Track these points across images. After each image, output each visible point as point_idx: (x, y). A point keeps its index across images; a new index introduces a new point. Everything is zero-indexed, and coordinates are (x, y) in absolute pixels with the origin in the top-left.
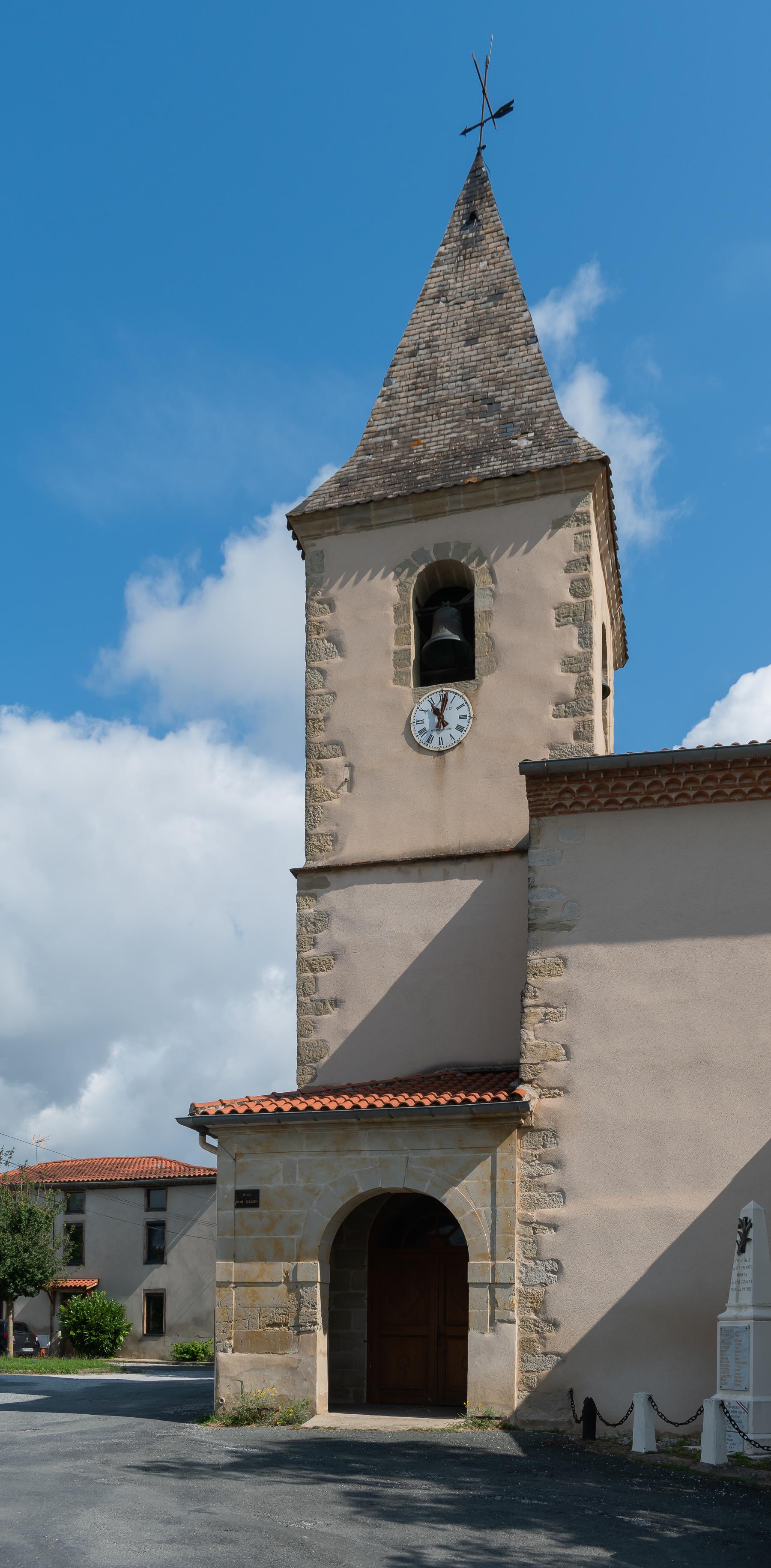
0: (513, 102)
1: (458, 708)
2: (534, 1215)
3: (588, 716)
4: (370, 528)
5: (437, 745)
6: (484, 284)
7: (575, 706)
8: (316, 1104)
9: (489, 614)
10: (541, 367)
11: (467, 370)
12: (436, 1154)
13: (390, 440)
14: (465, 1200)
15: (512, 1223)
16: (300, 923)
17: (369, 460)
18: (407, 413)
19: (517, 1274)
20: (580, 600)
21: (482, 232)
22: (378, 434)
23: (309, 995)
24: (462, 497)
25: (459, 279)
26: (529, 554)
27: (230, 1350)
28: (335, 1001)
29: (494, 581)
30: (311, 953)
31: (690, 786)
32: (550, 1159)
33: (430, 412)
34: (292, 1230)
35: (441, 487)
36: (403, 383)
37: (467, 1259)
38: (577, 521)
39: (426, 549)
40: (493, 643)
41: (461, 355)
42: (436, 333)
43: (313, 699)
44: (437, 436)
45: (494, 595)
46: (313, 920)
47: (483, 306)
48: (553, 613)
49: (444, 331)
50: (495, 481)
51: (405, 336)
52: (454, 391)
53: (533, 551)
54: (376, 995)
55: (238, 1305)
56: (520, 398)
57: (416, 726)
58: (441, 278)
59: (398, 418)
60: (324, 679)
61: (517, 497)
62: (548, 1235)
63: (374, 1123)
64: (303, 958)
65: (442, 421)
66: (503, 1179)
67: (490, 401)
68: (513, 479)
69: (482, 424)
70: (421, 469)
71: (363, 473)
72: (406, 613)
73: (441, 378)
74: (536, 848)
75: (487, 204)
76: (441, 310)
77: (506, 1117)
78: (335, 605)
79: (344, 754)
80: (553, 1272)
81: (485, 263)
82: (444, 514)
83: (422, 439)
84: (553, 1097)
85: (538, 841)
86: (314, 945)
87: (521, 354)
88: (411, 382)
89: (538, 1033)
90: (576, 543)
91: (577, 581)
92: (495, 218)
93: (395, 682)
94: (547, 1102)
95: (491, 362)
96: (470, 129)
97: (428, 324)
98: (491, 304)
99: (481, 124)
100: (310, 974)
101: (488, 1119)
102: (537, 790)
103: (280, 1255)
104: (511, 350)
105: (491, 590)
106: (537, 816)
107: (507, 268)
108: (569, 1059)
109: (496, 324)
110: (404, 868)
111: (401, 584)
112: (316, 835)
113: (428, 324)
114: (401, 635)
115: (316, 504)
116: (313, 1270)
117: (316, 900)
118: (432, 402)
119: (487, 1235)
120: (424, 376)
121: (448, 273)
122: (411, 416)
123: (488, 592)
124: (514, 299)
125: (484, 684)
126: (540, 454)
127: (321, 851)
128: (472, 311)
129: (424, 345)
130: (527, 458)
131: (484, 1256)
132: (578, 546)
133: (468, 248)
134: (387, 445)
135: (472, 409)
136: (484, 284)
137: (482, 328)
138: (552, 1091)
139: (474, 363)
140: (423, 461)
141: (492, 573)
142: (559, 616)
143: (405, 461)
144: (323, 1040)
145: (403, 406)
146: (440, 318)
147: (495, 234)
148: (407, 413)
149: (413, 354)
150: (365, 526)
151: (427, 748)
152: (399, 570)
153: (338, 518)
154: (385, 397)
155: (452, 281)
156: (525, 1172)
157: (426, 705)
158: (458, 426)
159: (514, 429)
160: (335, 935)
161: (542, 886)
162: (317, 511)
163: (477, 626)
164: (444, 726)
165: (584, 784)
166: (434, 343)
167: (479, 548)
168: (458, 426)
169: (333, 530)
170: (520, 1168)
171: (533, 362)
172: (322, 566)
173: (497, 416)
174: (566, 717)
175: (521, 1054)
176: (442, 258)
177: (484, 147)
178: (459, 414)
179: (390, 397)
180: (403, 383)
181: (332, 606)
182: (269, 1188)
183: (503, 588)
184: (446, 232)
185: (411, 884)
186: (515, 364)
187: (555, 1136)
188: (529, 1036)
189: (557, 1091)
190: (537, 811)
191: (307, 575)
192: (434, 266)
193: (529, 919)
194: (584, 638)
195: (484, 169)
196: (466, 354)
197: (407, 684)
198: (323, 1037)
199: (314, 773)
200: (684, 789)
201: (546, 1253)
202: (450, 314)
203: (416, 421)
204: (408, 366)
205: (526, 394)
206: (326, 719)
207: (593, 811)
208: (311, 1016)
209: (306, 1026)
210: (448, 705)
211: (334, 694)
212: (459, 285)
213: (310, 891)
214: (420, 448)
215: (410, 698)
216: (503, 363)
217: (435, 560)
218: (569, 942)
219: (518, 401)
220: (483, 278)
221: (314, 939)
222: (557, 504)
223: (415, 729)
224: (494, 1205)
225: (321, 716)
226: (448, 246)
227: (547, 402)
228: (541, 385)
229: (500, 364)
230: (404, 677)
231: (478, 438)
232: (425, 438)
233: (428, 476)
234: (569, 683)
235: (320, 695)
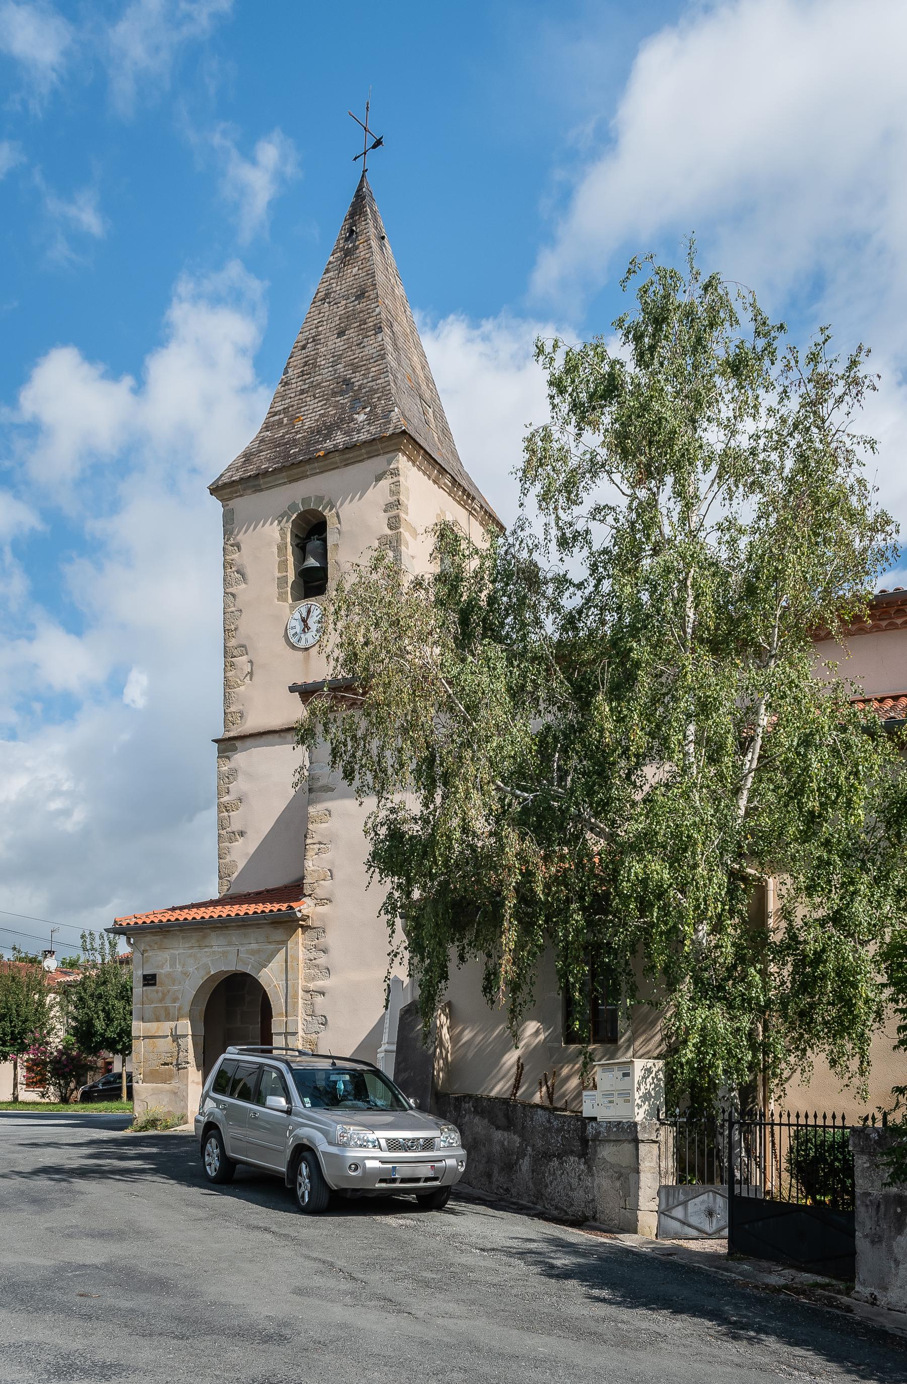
2: (311, 986)
4: (262, 490)
12: (254, 946)
14: (270, 977)
15: (297, 992)
19: (300, 1026)
21: (357, 243)
22: (275, 414)
27: (140, 1082)
30: (226, 799)
32: (321, 947)
34: (175, 1000)
36: (295, 372)
37: (271, 1017)
42: (320, 329)
54: (266, 826)
55: (145, 1051)
62: (319, 999)
65: (317, 400)
73: (319, 366)
80: (322, 1024)
82: (307, 477)
94: (320, 909)
97: (316, 322)
98: (357, 302)
99: (365, 153)
100: (226, 814)
101: (281, 923)
103: (168, 1018)
110: (282, 734)
113: (316, 322)
114: (283, 565)
115: (225, 479)
116: (185, 1026)
119: (283, 1001)
122: (297, 398)
123: (336, 530)
131: (281, 1014)
132: (392, 493)
134: (280, 422)
141: (338, 516)
150: (258, 489)
152: (280, 519)
155: (334, 285)
156: (306, 957)
160: (239, 786)
168: (325, 404)
175: (303, 878)
176: (330, 266)
179: (286, 384)
180: (295, 372)
182: (162, 972)
183: (345, 527)
197: (286, 601)
199: (229, 668)
201: (318, 1012)
206: (236, 629)
208: (227, 844)
212: (338, 288)
218: (332, 799)
219: (365, 381)
222: (376, 464)
223: (291, 632)
224: (287, 980)
225: (233, 627)
226: (336, 256)
228: (381, 367)
229: (357, 352)
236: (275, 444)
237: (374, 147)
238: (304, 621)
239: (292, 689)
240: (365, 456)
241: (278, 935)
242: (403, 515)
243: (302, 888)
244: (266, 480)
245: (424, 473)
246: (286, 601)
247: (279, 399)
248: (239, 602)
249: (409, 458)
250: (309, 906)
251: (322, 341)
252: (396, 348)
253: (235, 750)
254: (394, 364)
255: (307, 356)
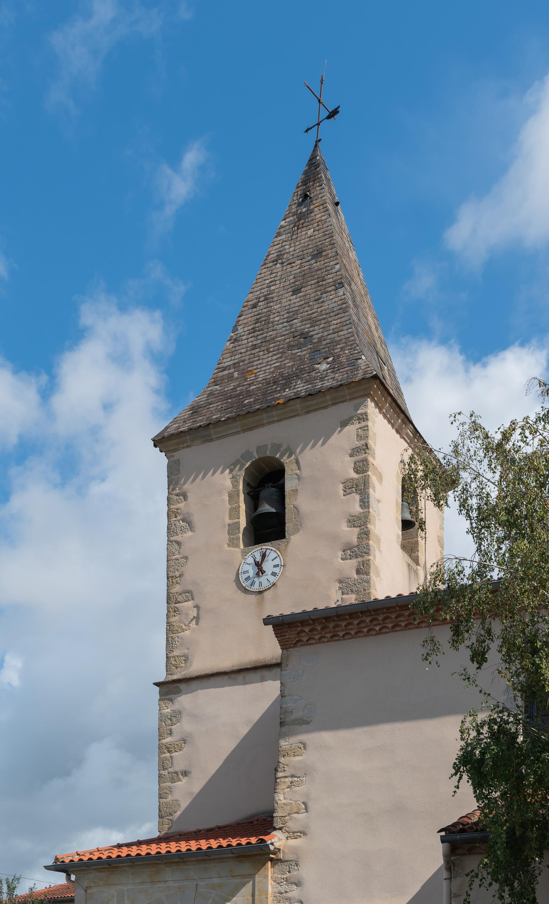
0: (339, 107)
1: (272, 560)
3: (366, 557)
4: (212, 440)
5: (258, 587)
6: (310, 246)
7: (359, 550)
8: (173, 847)
9: (295, 491)
10: (344, 306)
11: (292, 314)
12: (216, 881)
13: (233, 373)
16: (161, 720)
17: (216, 390)
18: (247, 351)
20: (361, 475)
21: (312, 207)
22: (224, 369)
23: (167, 769)
24: (274, 413)
25: (292, 245)
26: (324, 447)
28: (185, 772)
29: (299, 469)
30: (168, 740)
31: (388, 621)
32: (293, 880)
33: (262, 349)
35: (259, 409)
36: (246, 329)
38: (358, 420)
39: (251, 451)
40: (298, 512)
41: (289, 302)
42: (273, 288)
43: (172, 563)
44: (265, 366)
45: (299, 478)
46: (169, 717)
47: (308, 263)
48: (341, 486)
49: (278, 286)
50: (297, 400)
51: (250, 293)
52: (281, 331)
53: (326, 445)
56: (326, 331)
57: (243, 575)
58: (280, 245)
59: (240, 355)
60: (180, 548)
61: (314, 408)
63: (174, 862)
64: (163, 744)
65: (270, 354)
66: (260, 895)
67: (306, 336)
68: (310, 397)
69: (298, 354)
70: (249, 394)
71: (210, 401)
72: (237, 497)
73: (272, 322)
74: (286, 670)
75: (318, 184)
76: (278, 270)
77: (260, 854)
78: (187, 496)
79: (193, 599)
81: (312, 230)
82: (263, 425)
83: (255, 369)
84: (296, 838)
85: (287, 665)
86: (170, 734)
87: (331, 297)
88: (252, 327)
89: (286, 796)
90: (358, 435)
91: (358, 462)
92: (322, 195)
93: (229, 545)
94: (292, 842)
95: (309, 306)
96: (311, 128)
97: (267, 282)
98: (313, 261)
99: (318, 124)
100: (168, 755)
101: (248, 856)
102: (281, 633)
104: (324, 295)
105: (297, 474)
106: (286, 649)
107: (327, 233)
108: (307, 812)
109: (316, 277)
111: (233, 477)
112: (174, 657)
113: (267, 282)
115: (171, 431)
117: (172, 702)
118: (265, 341)
120: (261, 322)
121: (285, 241)
122: (249, 353)
123: (295, 476)
124: (330, 255)
125: (292, 541)
126: (332, 375)
127: (177, 668)
128: (299, 268)
129: (263, 298)
130: (322, 379)
133: (301, 219)
134: (230, 377)
135: (292, 343)
136: (310, 246)
137: (305, 280)
138: (296, 834)
139: (297, 308)
140: (251, 388)
141: (297, 462)
142: (345, 488)
143: (240, 388)
144: (176, 800)
145: (244, 346)
146: (276, 276)
147: (321, 207)
148: (247, 351)
149: (255, 306)
150: (208, 439)
151: (251, 590)
152: (232, 467)
153: (188, 437)
154: (232, 341)
155: (287, 247)
156: (276, 890)
157: (250, 560)
158: (281, 357)
159: (320, 355)
161: (289, 695)
162: (172, 435)
163: (287, 500)
164: (262, 573)
165: (313, 626)
166: (270, 296)
167: (288, 446)
168: (281, 357)
169: (185, 445)
170: (271, 887)
171: (339, 302)
172: (179, 470)
173: (309, 346)
174: (350, 559)
175: (273, 811)
176: (282, 230)
177: (320, 140)
178: (282, 348)
179: (236, 340)
180: (246, 329)
181: (185, 496)
183: (305, 472)
184: (287, 210)
185: (238, 687)
186: (326, 306)
187: (297, 865)
188: (281, 798)
189: (299, 834)
190: (284, 645)
191: (168, 477)
192: (276, 237)
193: (280, 718)
194: (364, 502)
195: (318, 158)
196: (292, 302)
197: (237, 546)
198: (176, 798)
200: (383, 623)
202: (284, 272)
203: (252, 356)
204: (250, 315)
205: (332, 327)
206: (180, 576)
207: (324, 642)
209: (164, 791)
210: (266, 558)
211: (186, 558)
212: (292, 249)
213: (168, 697)
214: (252, 377)
215: (239, 556)
216: (318, 306)
217: (257, 457)
219: (326, 334)
220: (309, 243)
221: (171, 730)
222: (344, 409)
223: (242, 577)
225: (177, 574)
226: (287, 220)
227: (346, 332)
228: (343, 319)
229: (315, 307)
230: (235, 542)
231: (293, 365)
232: (257, 369)
233: (252, 400)
234: (352, 535)
235: (177, 559)
236: (225, 396)
237: (329, 117)
238: (258, 565)
239: (267, 621)
240: (330, 403)
241: (245, 868)
242: (370, 459)
243: (272, 821)
244: (218, 429)
245: (389, 422)
246: (237, 546)
247: (229, 355)
248: (185, 550)
249: (377, 405)
250: (280, 840)
251: (275, 299)
252: (356, 306)
253: (178, 692)
254: (356, 320)
255: (259, 314)
